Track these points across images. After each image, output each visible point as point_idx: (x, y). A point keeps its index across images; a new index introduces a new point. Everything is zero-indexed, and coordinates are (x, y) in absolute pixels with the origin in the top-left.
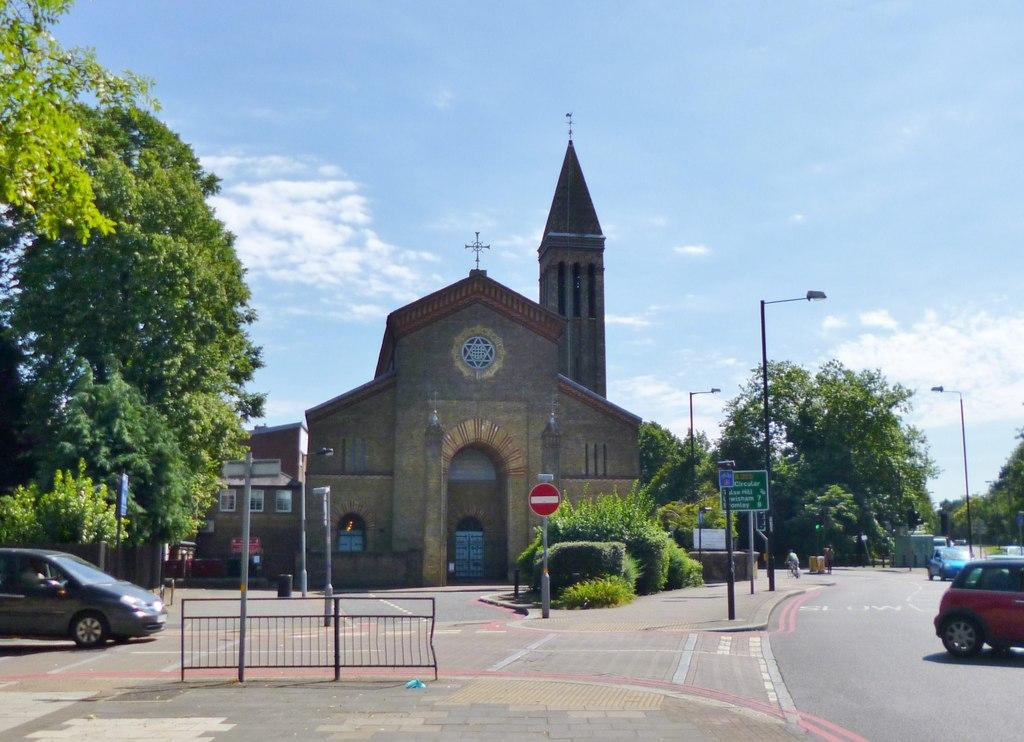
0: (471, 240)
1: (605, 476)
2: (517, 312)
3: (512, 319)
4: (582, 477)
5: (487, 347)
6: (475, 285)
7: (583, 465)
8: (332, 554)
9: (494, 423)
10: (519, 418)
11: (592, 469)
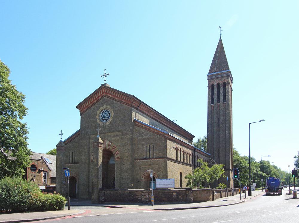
0: (107, 72)
1: (153, 158)
3: (116, 100)
4: (144, 159)
5: (105, 112)
6: (103, 90)
7: (145, 155)
9: (110, 141)
10: (118, 138)
11: (148, 156)
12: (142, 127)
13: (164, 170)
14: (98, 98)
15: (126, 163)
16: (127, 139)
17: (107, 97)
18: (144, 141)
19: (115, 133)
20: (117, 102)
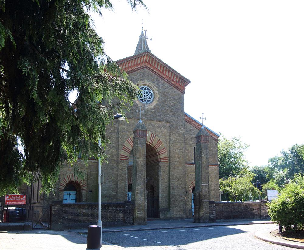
2: (165, 75)
3: (162, 78)
6: (145, 58)
8: (79, 202)
10: (165, 131)
12: (190, 123)
13: (215, 180)
14: (135, 65)
15: (178, 167)
16: (179, 134)
17: (149, 69)
18: (192, 141)
19: (160, 123)
20: (164, 81)
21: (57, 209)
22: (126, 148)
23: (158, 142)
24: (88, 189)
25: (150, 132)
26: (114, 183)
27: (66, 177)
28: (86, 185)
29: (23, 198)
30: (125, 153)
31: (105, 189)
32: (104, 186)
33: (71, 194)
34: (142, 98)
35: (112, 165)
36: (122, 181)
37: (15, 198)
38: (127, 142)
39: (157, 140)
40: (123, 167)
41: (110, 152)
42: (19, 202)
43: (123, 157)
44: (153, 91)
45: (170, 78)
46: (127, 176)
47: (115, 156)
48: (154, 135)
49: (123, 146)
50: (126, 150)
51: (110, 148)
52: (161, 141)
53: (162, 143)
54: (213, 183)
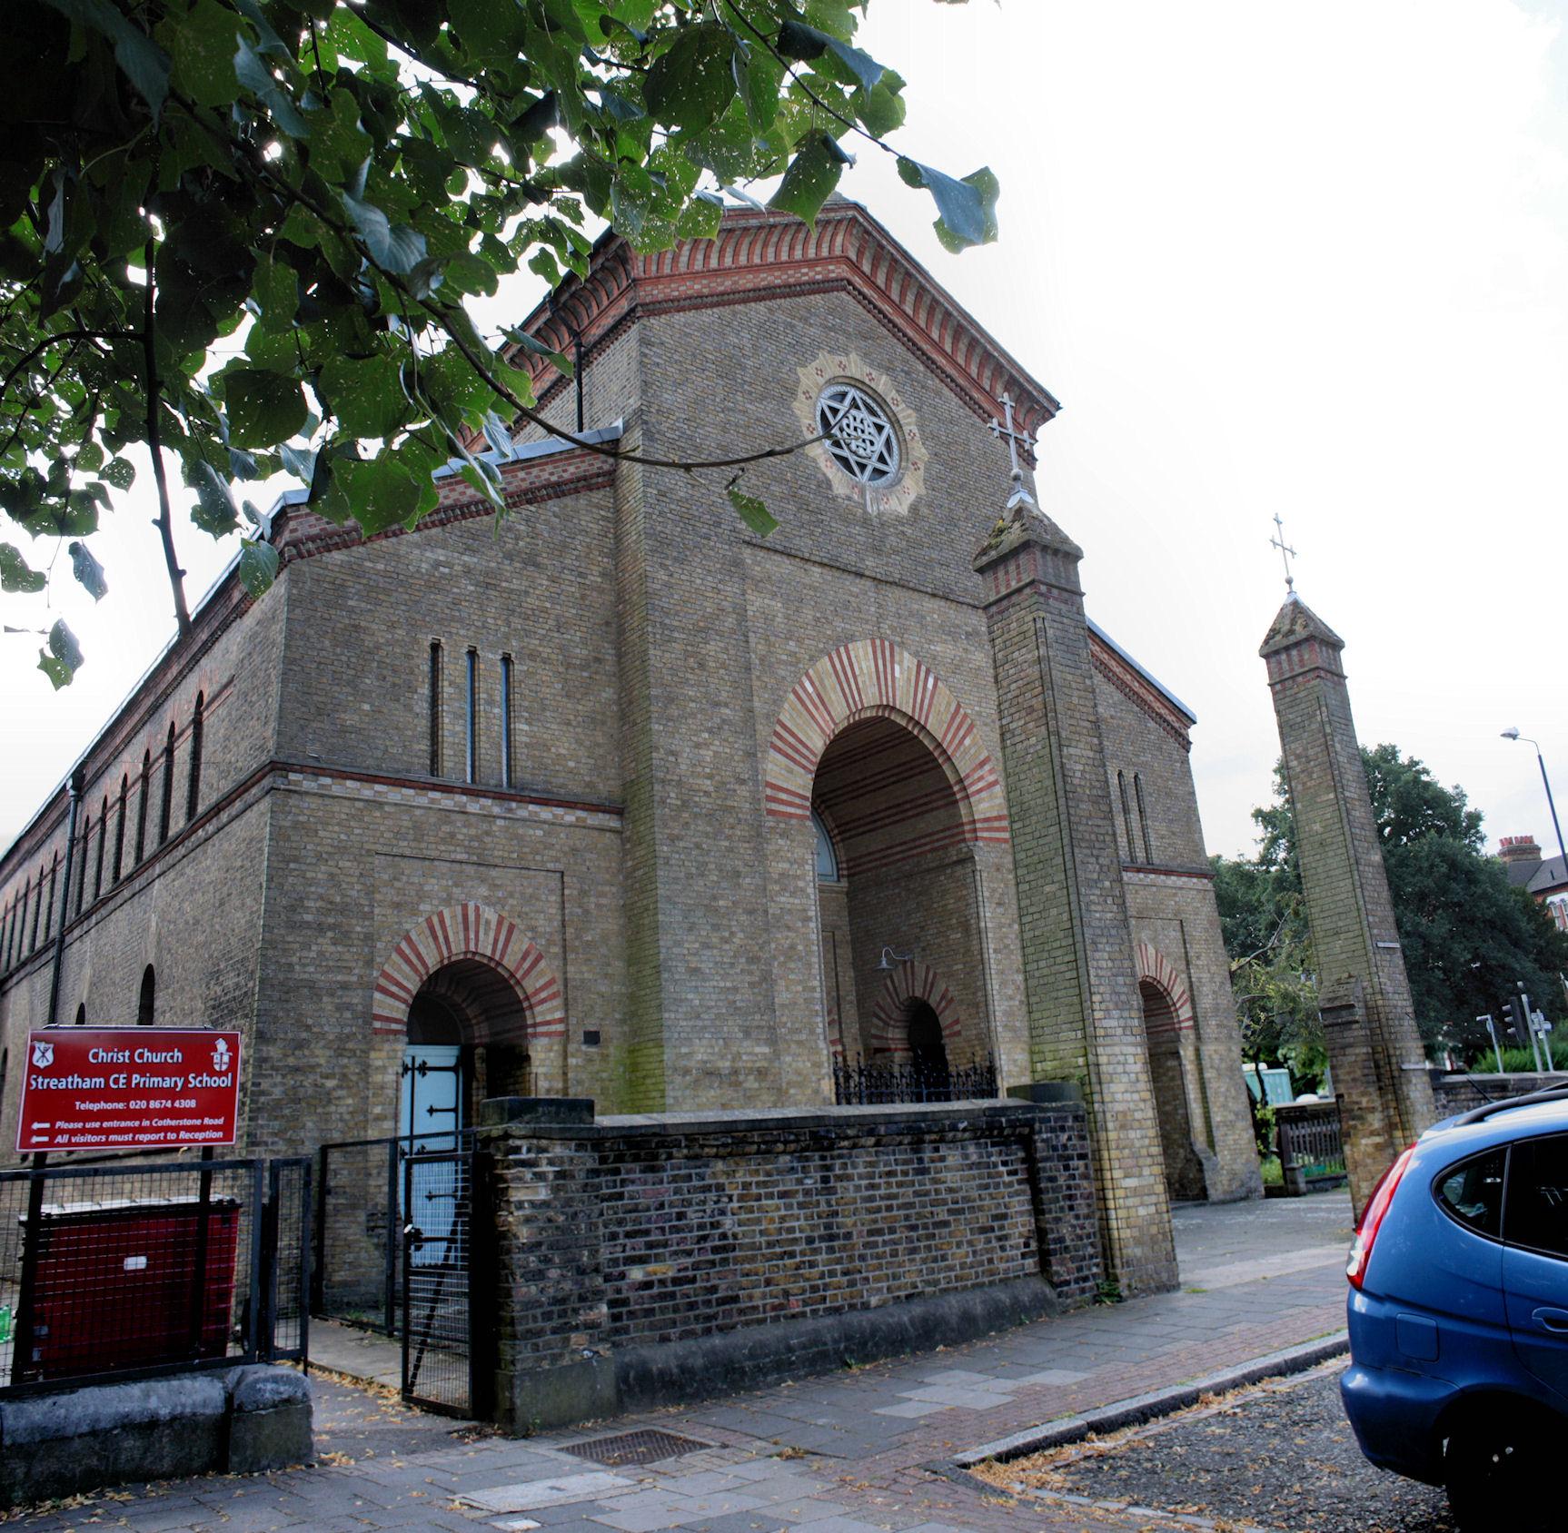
21: (556, 1189)
22: (791, 740)
23: (953, 719)
24: (573, 1021)
25: (906, 654)
26: (751, 973)
27: (416, 928)
28: (554, 989)
29: (212, 1073)
30: (791, 771)
31: (698, 1017)
32: (690, 996)
33: (424, 1069)
34: (845, 453)
35: (730, 850)
36: (790, 958)
37: (131, 1068)
38: (799, 706)
39: (947, 710)
40: (786, 866)
41: (707, 754)
42: (164, 1113)
43: (783, 796)
44: (895, 422)
45: (964, 372)
46: (812, 925)
47: (743, 791)
48: (928, 672)
49: (778, 729)
50: (797, 757)
51: (710, 731)
52: (965, 716)
53: (971, 726)
54: (1205, 976)
